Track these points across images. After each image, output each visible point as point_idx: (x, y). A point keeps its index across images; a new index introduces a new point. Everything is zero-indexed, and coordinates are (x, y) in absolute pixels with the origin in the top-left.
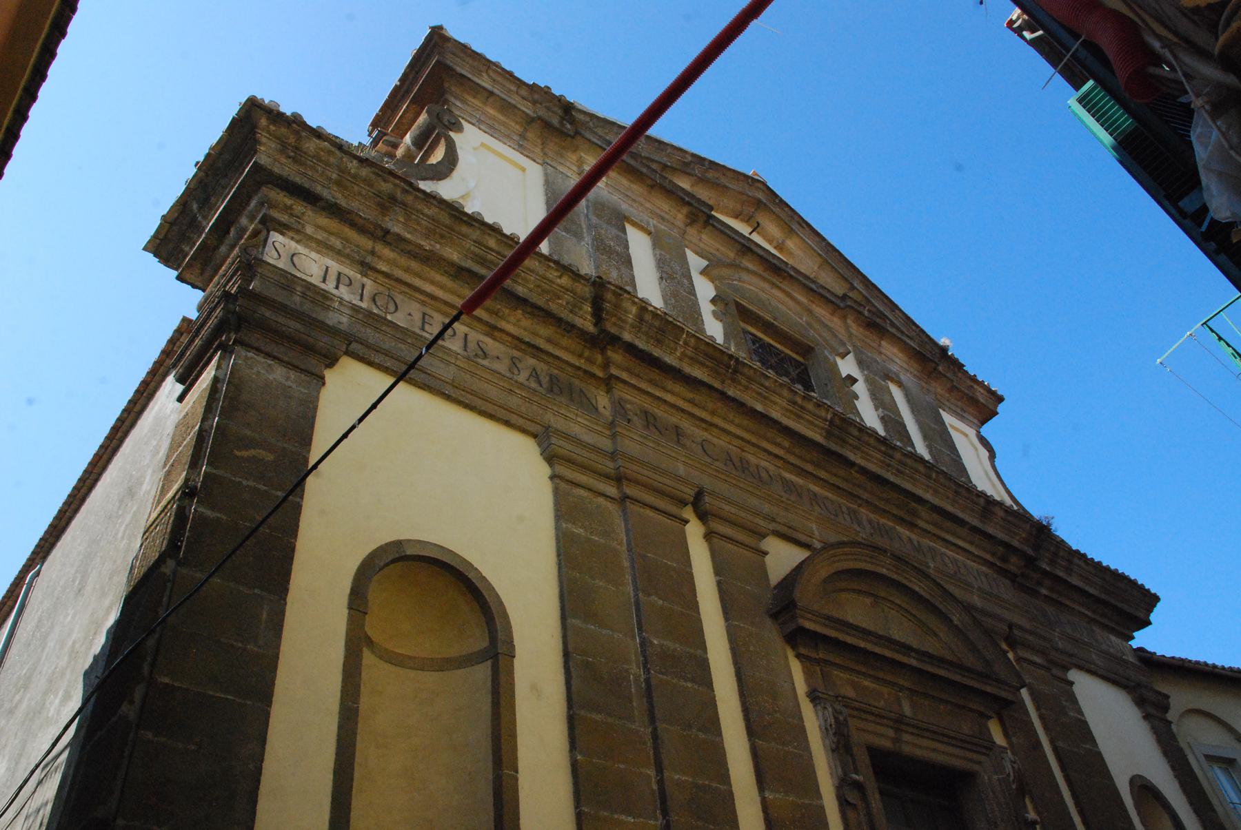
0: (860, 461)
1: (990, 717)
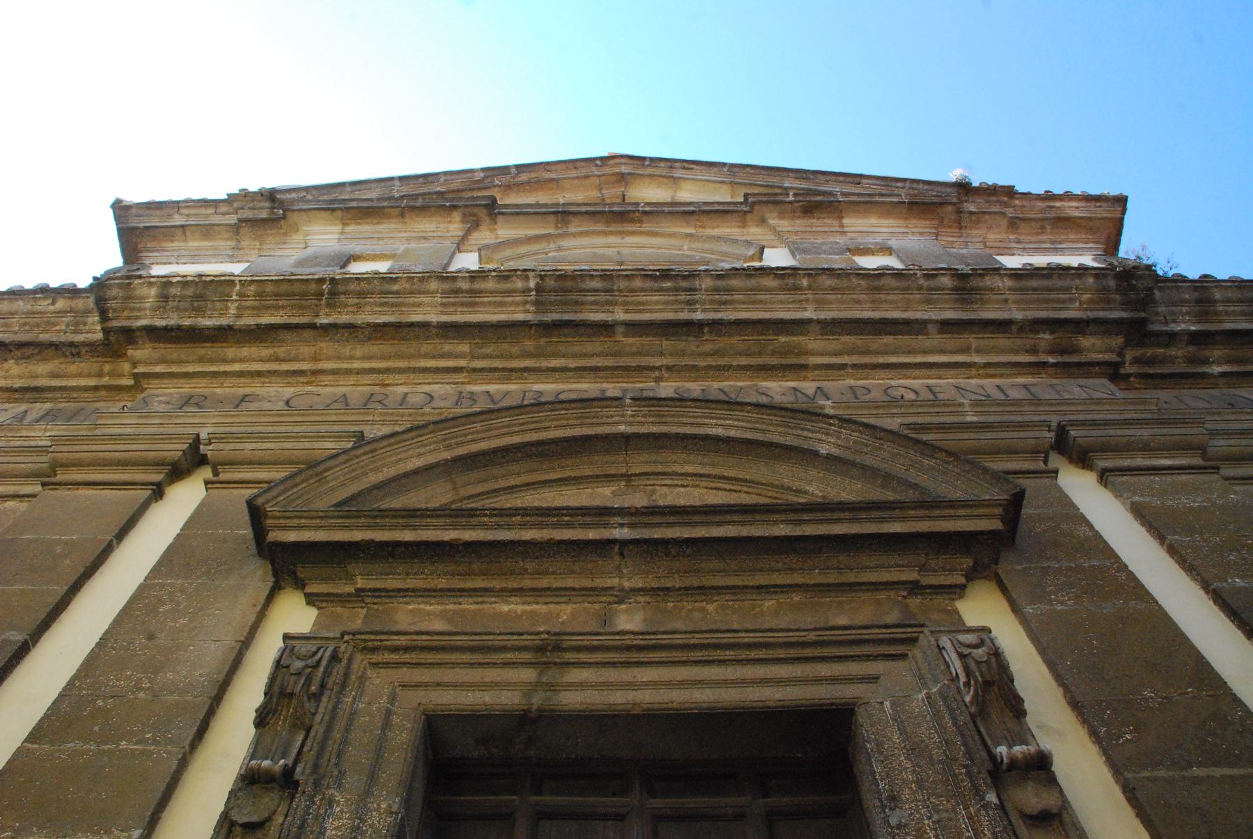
0: (620, 315)
1: (958, 591)
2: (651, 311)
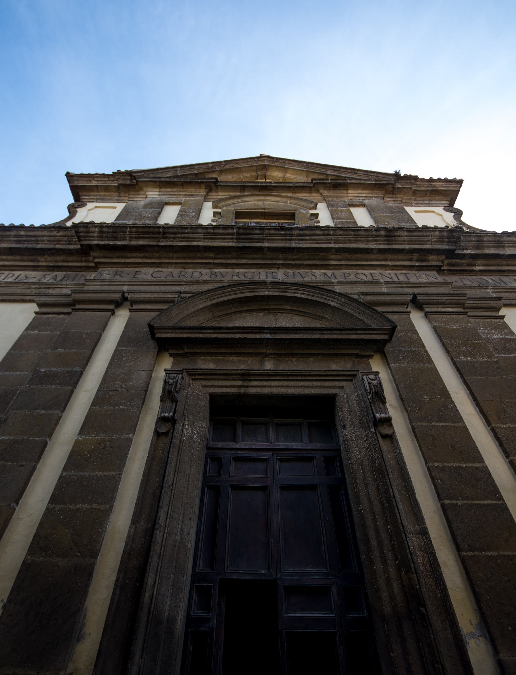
1: (371, 357)
2: (276, 243)
